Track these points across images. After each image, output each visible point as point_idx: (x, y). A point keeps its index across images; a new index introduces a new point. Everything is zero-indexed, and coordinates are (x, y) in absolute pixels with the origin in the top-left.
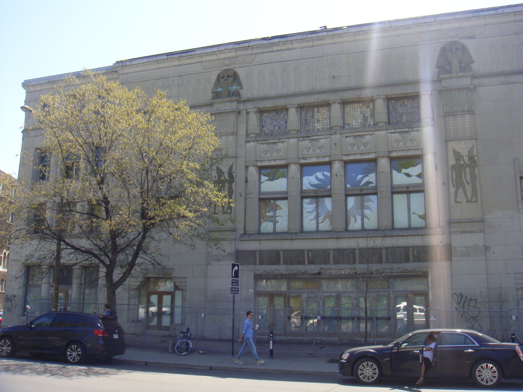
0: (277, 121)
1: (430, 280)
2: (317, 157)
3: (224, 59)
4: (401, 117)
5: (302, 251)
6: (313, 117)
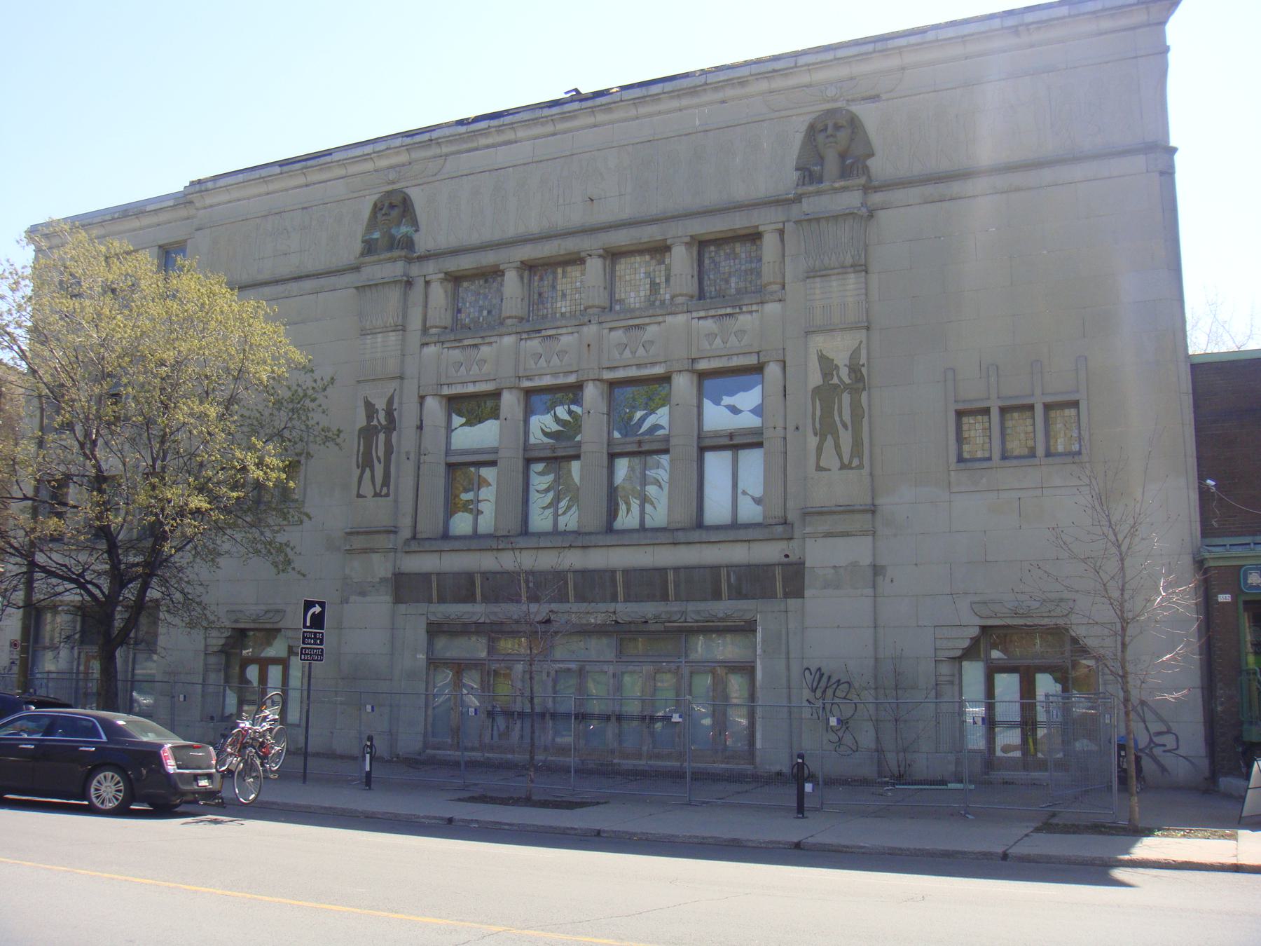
0: (486, 297)
1: (759, 639)
2: (555, 374)
4: (727, 281)
6: (554, 287)
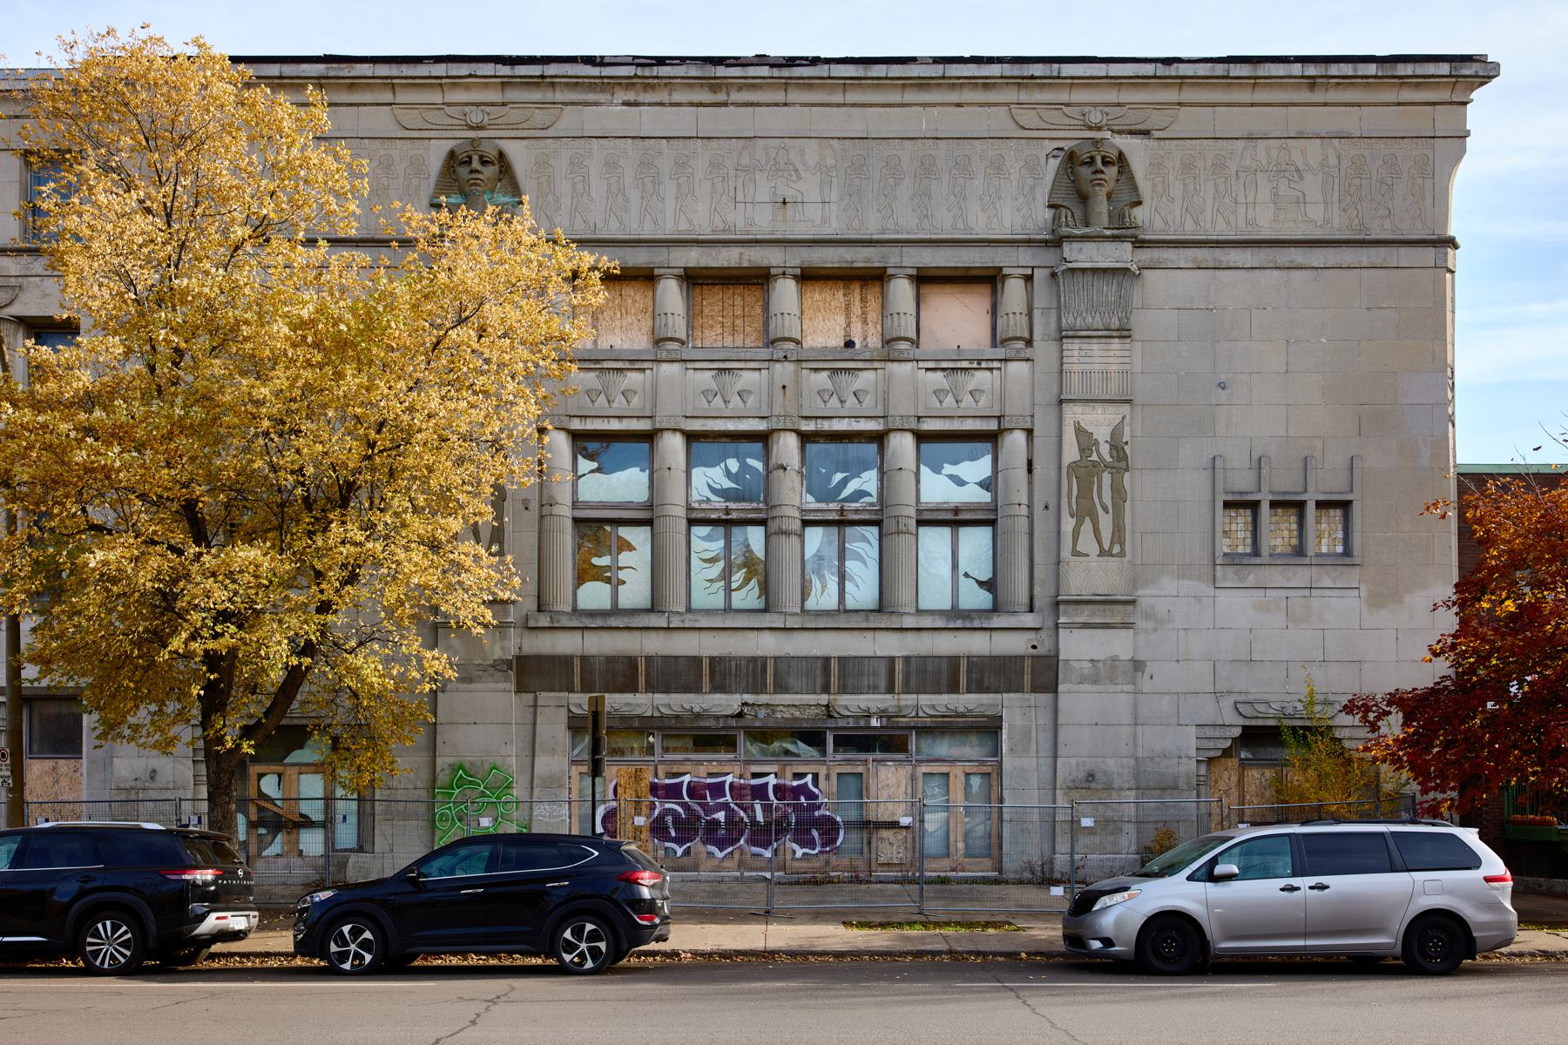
3: (467, 104)
5: (696, 661)
